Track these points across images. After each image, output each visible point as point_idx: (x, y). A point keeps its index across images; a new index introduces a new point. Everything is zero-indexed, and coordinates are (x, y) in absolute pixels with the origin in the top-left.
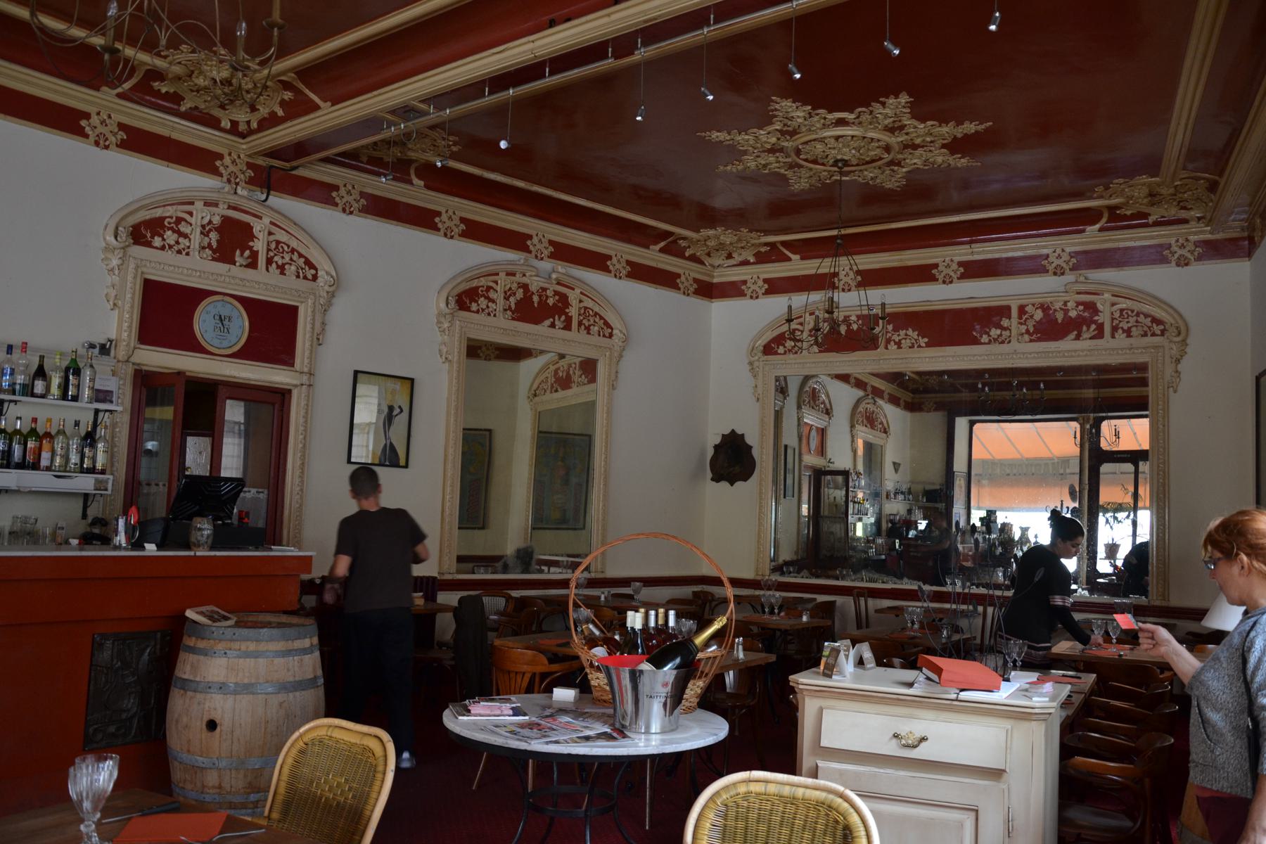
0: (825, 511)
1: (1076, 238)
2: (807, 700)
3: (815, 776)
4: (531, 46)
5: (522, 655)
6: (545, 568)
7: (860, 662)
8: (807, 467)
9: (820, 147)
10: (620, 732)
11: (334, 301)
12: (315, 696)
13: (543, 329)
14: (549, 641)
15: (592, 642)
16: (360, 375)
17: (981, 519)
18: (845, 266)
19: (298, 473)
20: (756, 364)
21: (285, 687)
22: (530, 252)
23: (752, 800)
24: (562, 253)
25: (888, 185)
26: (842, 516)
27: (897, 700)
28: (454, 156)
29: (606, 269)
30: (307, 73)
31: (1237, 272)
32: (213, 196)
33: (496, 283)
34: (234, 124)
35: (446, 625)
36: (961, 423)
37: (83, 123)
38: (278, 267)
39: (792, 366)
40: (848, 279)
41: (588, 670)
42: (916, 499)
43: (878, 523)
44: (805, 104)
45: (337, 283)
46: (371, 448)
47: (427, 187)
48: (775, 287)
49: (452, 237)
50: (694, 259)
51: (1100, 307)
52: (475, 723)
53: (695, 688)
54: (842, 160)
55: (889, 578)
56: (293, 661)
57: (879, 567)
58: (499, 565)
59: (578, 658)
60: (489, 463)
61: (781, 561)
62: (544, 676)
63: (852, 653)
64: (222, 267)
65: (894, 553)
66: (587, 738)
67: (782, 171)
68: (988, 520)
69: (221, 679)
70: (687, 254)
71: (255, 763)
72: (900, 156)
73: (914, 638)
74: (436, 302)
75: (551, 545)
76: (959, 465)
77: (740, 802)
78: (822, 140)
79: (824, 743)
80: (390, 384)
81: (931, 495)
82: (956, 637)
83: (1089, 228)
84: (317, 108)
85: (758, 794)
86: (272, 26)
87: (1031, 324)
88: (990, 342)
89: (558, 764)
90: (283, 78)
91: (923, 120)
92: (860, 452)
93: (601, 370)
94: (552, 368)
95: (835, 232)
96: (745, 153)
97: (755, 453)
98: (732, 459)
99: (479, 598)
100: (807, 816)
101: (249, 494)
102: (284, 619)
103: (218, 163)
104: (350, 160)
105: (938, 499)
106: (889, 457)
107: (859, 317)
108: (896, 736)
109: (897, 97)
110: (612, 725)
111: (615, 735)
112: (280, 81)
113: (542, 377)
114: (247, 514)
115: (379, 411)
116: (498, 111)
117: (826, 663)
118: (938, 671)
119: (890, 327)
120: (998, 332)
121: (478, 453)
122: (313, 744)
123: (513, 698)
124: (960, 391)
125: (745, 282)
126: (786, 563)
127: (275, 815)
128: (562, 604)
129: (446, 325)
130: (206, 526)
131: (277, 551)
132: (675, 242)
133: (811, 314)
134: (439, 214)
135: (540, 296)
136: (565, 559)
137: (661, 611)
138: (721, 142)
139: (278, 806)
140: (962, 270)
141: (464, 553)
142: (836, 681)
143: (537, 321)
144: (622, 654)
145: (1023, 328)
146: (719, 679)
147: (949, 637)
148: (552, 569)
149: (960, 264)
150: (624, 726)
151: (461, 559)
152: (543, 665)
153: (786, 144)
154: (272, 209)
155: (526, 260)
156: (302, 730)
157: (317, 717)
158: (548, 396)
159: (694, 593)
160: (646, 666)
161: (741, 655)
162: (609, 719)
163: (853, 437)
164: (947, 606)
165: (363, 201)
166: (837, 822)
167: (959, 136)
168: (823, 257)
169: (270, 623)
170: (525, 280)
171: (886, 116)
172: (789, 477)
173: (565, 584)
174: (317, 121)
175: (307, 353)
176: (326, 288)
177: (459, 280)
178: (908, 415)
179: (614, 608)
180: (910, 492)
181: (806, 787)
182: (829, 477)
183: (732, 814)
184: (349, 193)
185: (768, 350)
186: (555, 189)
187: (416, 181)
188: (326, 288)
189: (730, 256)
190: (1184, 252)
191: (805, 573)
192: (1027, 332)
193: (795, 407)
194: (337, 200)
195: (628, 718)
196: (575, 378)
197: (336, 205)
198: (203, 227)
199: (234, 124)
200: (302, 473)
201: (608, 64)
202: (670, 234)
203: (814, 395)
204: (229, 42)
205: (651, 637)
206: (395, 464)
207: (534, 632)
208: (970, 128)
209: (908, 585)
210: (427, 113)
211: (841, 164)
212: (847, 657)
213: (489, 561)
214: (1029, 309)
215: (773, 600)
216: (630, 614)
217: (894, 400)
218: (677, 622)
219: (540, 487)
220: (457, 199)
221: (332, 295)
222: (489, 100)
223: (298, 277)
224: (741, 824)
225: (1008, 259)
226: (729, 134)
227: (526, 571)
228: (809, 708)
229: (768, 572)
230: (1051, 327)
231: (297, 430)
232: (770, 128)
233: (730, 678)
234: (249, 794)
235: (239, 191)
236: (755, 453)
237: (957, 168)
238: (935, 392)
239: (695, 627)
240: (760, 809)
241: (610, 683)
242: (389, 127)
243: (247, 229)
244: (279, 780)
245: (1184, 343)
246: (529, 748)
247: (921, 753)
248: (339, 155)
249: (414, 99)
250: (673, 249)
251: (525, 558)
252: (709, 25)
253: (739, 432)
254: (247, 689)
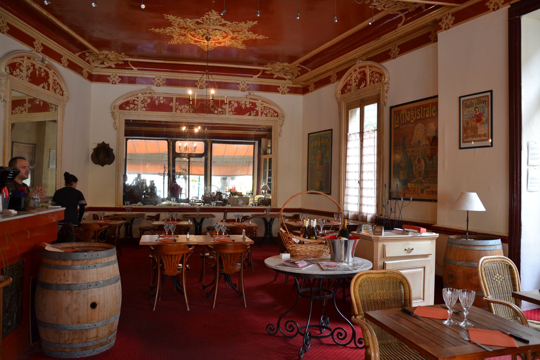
1: (250, 79)
16: (14, 143)
20: (116, 113)
24: (47, 51)
31: (299, 98)
33: (23, 61)
37: (278, 89)
51: (257, 105)
83: (254, 76)
87: (233, 109)
88: (129, 110)
95: (205, 64)
107: (164, 98)
119: (178, 103)
120: (133, 106)
125: (109, 76)
143: (38, 84)
145: (143, 105)
170: (34, 62)
185: (121, 107)
190: (202, 84)
214: (233, 102)
230: (240, 110)
245: (283, 120)
247: (413, 253)
253: (106, 143)
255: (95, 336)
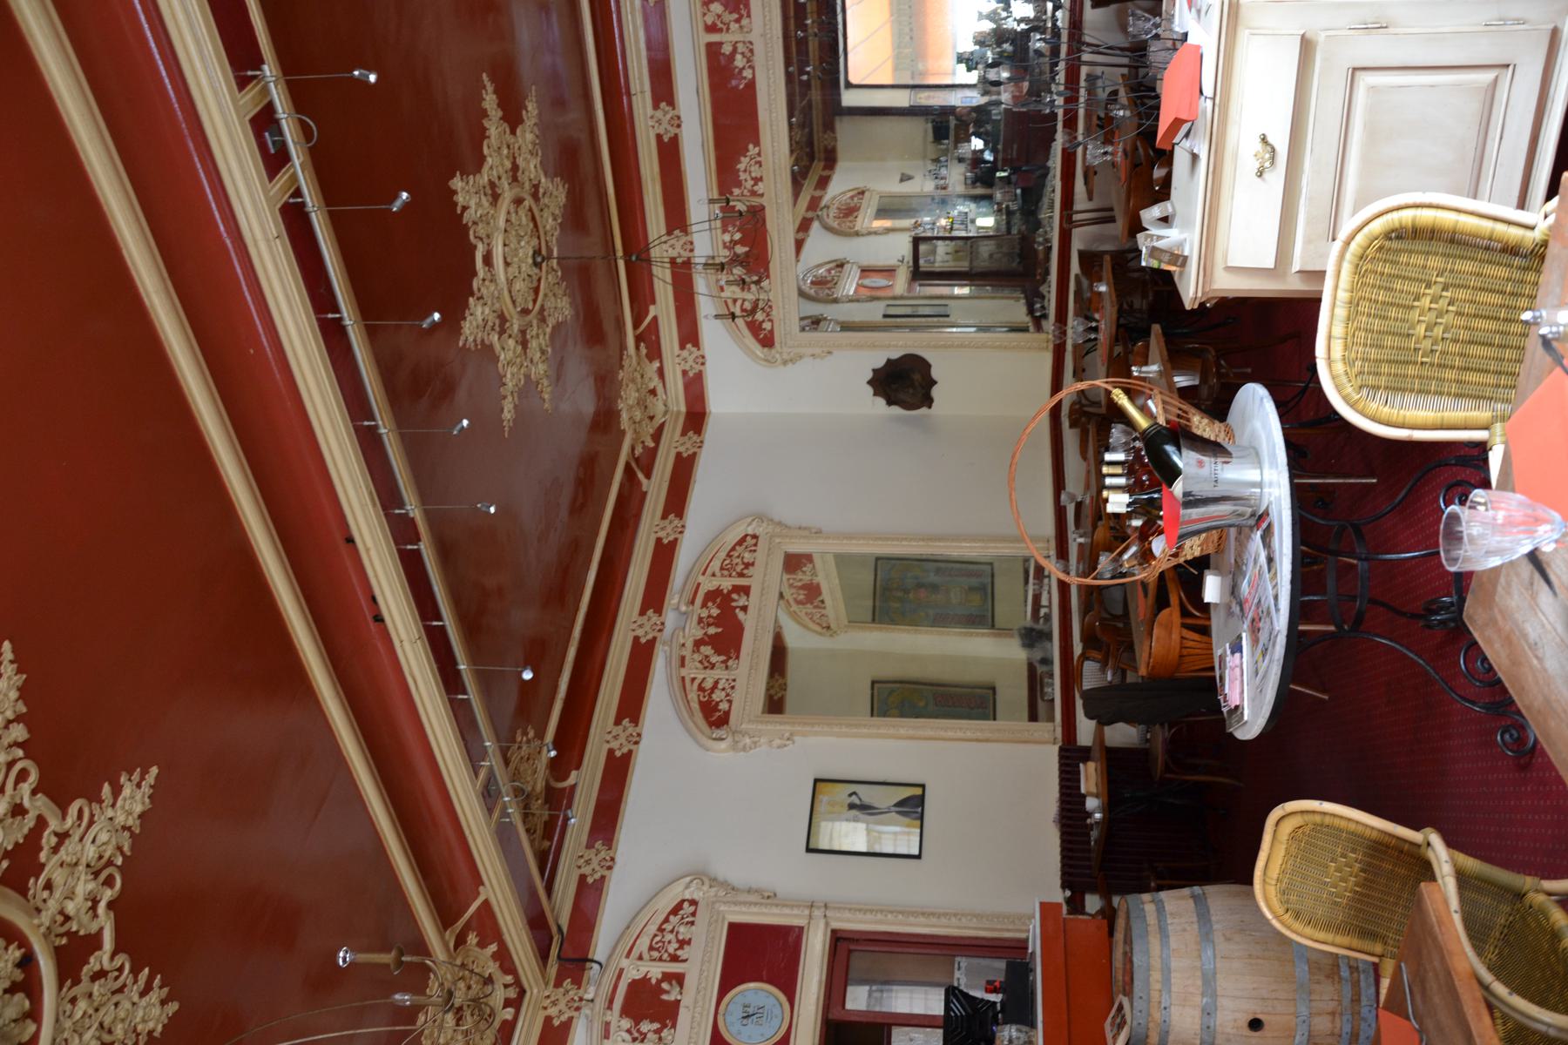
0: (963, 266)
2: (1216, 286)
3: (1321, 275)
4: (407, 645)
5: (1161, 641)
6: (1043, 611)
7: (1165, 220)
8: (910, 289)
9: (518, 285)
10: (1261, 518)
11: (721, 877)
12: (1218, 896)
13: (748, 621)
14: (1141, 607)
15: (1146, 556)
16: (812, 846)
17: (969, 69)
18: (663, 250)
19: (934, 920)
20: (785, 356)
21: (1206, 935)
22: (655, 639)
23: (1353, 355)
25: (562, 199)
26: (970, 244)
27: (1215, 173)
28: (540, 735)
29: (673, 544)
30: (446, 915)
32: (597, 1028)
33: (693, 680)
34: (508, 1003)
35: (1123, 734)
36: (849, 99)
38: (681, 948)
39: (787, 312)
40: (678, 245)
41: (1181, 560)
42: (945, 152)
43: (976, 199)
44: (466, 306)
45: (700, 875)
46: (897, 829)
47: (578, 767)
48: (690, 335)
49: (639, 735)
50: (657, 436)
52: (1252, 700)
53: (1201, 425)
54: (534, 257)
55: (1048, 183)
56: (1173, 924)
57: (1032, 197)
58: (1040, 669)
59: (1162, 574)
60: (931, 684)
61: (1027, 319)
62: (1185, 613)
63: (1154, 231)
64: (684, 1016)
65: (1014, 178)
66: (1270, 560)
67: (548, 330)
68: (969, 61)
69: (1197, 1013)
70: (652, 445)
71: (1302, 970)
72: (527, 185)
73: (1125, 152)
74: (720, 754)
75: (1013, 604)
76: (901, 99)
77: (1356, 370)
78: (510, 283)
79: (1270, 264)
80: (821, 808)
81: (940, 133)
82: (1123, 96)
84: (486, 903)
85: (1346, 347)
86: (400, 963)
87: (729, 17)
88: (752, 67)
89: (1304, 593)
90: (452, 945)
91: (481, 159)
92: (887, 223)
93: (797, 547)
94: (795, 607)
96: (527, 377)
97: (895, 355)
98: (904, 383)
99: (1086, 696)
100: (1374, 286)
101: (961, 979)
102: (1119, 936)
103: (556, 1023)
104: (547, 861)
105: (945, 126)
106: (896, 188)
107: (725, 231)
108: (1260, 174)
109: (455, 192)
110: (1251, 528)
111: (1264, 525)
112: (456, 947)
113: (807, 620)
114: (988, 982)
115: (856, 820)
116: (486, 682)
117: (1169, 263)
118: (1178, 123)
119: (736, 191)
120: (739, 57)
121: (902, 698)
122: (1287, 902)
123: (1218, 652)
124: (810, 102)
125: (685, 373)
126: (1031, 311)
127: (1378, 949)
128: (1089, 593)
129: (748, 741)
130: (1006, 1033)
131: (1035, 946)
132: (637, 460)
133: (722, 289)
134: (611, 752)
135: (709, 625)
136: (1031, 588)
137: (1105, 470)
138: (516, 407)
139: (1367, 945)
140: (663, 105)
141: (1026, 714)
142: (1191, 250)
143: (739, 629)
144: (1161, 518)
145: (734, 26)
146: (1184, 393)
147: (1123, 107)
148: (1044, 602)
149: (656, 106)
150: (1253, 515)
151: (1033, 717)
152: (1171, 614)
153: (516, 327)
154: (610, 956)
155: (664, 643)
156: (1269, 915)
157: (1251, 895)
158: (829, 611)
159: (1071, 426)
160: (1178, 488)
161: (1154, 368)
162: (1243, 533)
163: (870, 233)
164: (1081, 112)
165: (598, 844)
166: (1381, 248)
167: (500, 113)
168: (651, 275)
169: (1125, 953)
170: (690, 644)
171: (479, 205)
172: (922, 311)
173: (1064, 587)
174: (502, 903)
175: (787, 911)
176: (705, 888)
177: (691, 724)
178: (841, 166)
179: (1095, 527)
180: (936, 161)
181: (1336, 287)
182: (921, 262)
183: (1371, 380)
184: (588, 862)
185: (767, 341)
186: (577, 609)
187: (571, 781)
188: (705, 888)
189: (653, 392)
191: (1043, 289)
192: (738, 21)
193: (835, 306)
194: (597, 876)
195: (1241, 509)
196: (806, 578)
197: (603, 877)
198: (634, 1040)
199: (508, 1003)
200: (933, 914)
201: (426, 548)
202: (628, 468)
203: (819, 282)
204: (410, 1014)
205: (1139, 483)
206: (920, 801)
207: (1128, 624)
208: (490, 101)
209: (1056, 162)
210: (491, 768)
211: (539, 258)
212: (1160, 238)
213: (1035, 682)
214: (709, 20)
215: (1081, 329)
216: (1110, 508)
217: (823, 183)
218: (1114, 450)
219: (941, 620)
220: (592, 731)
221: (714, 881)
222: (473, 694)
223: (692, 923)
224: (1385, 368)
225: (649, 48)
226: (505, 397)
227: (1049, 636)
228: (1227, 284)
229: (1042, 336)
231: (880, 922)
232: (497, 347)
233: (1181, 381)
234: (1340, 978)
235: (589, 996)
236: (895, 354)
237: (540, 115)
238: (811, 134)
239: (1120, 426)
240: (1365, 345)
241: (1198, 533)
242: (508, 815)
243: (634, 985)
244: (1333, 944)
246: (1284, 632)
247: (1281, 143)
248: (542, 874)
249: (474, 786)
250: (646, 463)
251: (1033, 637)
252: (376, 427)
253: (870, 375)
254: (1209, 981)
255: (1329, 1018)
